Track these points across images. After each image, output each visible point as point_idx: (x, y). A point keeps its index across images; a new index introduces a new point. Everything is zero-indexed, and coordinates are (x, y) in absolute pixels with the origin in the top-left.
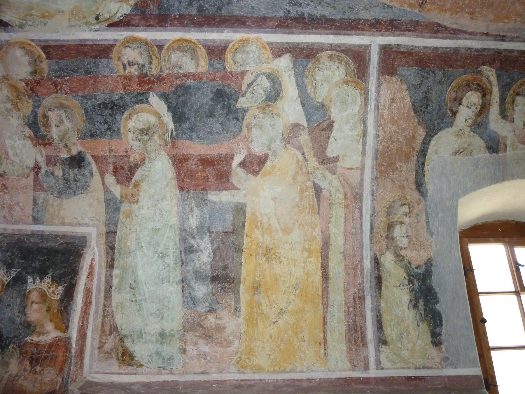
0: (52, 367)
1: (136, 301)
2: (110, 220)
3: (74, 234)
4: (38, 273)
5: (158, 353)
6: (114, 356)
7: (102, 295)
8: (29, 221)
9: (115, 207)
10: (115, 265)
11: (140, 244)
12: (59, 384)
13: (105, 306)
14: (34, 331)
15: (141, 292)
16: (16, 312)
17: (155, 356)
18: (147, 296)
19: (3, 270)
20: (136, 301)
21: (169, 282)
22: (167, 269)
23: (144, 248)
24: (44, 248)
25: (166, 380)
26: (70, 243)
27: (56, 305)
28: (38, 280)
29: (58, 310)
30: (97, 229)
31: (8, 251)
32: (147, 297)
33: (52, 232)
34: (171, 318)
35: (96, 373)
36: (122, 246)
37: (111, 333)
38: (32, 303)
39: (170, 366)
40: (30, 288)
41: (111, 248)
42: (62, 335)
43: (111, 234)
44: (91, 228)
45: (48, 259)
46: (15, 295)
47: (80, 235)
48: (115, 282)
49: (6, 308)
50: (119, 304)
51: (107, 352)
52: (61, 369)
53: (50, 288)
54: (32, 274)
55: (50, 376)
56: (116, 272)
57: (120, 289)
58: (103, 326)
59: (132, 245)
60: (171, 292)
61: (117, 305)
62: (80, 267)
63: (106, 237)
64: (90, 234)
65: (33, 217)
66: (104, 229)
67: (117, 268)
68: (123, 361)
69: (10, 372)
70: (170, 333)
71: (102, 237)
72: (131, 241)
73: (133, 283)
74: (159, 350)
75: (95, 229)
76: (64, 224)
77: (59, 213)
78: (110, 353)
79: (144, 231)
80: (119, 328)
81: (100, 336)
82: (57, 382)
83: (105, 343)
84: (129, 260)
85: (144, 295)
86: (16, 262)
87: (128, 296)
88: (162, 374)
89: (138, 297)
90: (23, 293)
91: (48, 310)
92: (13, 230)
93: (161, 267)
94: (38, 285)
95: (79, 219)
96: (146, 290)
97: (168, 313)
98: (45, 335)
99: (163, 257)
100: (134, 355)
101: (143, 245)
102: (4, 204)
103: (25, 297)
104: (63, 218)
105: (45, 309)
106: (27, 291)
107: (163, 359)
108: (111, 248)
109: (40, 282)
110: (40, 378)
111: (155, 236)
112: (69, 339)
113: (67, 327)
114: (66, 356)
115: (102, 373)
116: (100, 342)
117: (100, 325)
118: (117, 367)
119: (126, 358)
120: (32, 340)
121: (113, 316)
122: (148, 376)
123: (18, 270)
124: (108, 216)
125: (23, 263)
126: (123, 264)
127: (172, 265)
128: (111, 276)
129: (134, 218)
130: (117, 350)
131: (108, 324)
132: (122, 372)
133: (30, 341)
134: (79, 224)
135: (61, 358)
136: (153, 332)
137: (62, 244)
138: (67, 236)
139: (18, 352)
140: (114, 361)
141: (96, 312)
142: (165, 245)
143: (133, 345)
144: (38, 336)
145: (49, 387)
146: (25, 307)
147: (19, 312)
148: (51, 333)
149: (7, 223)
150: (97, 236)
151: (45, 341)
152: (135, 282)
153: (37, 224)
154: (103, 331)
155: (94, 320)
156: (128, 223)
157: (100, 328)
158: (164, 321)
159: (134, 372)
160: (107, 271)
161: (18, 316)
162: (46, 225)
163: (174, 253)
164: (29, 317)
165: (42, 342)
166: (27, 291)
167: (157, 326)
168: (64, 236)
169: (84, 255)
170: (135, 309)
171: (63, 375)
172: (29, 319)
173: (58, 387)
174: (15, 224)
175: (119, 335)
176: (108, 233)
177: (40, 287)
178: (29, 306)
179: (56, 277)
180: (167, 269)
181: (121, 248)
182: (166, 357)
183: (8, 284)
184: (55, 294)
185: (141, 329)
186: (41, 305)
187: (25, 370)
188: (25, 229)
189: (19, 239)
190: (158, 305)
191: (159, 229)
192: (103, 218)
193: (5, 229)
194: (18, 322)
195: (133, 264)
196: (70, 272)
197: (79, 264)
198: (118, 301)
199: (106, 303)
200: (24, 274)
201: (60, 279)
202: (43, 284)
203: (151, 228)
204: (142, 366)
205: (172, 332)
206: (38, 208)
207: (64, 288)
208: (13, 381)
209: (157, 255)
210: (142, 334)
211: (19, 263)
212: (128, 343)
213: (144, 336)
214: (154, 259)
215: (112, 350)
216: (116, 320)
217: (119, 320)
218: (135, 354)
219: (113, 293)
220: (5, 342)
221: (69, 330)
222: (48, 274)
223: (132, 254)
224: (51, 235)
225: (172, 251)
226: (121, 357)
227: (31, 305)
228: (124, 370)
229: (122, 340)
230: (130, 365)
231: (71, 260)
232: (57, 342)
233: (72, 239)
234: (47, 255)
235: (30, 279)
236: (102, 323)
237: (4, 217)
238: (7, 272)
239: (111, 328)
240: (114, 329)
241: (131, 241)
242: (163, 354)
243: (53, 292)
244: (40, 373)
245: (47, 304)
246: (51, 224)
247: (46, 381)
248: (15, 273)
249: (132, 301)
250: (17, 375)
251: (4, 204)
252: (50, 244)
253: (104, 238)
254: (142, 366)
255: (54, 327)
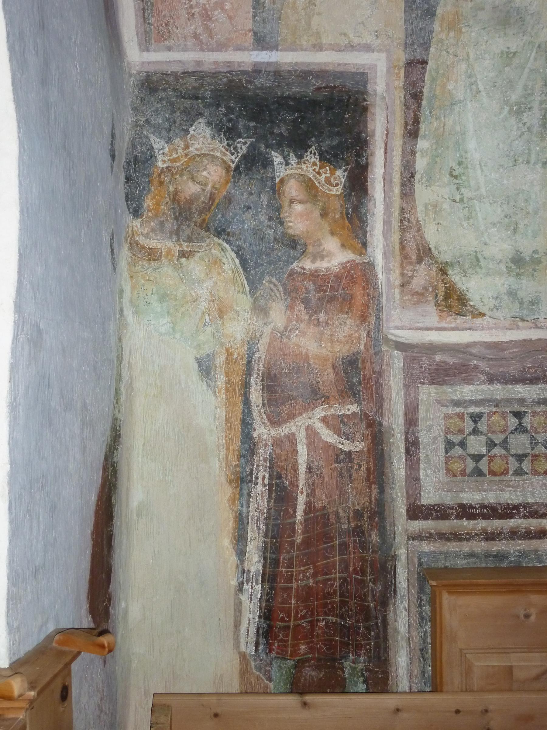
0: (347, 313)
1: (462, 200)
2: (414, 37)
3: (341, 69)
4: (289, 146)
5: (512, 293)
6: (430, 298)
7: (397, 190)
8: (247, 44)
9: (426, 6)
10: (421, 132)
11: (474, 87)
12: (363, 343)
13: (402, 210)
14: (304, 252)
15: (472, 183)
16: (263, 218)
17: (506, 297)
18: (483, 191)
19: (221, 142)
20: (462, 200)
21: (528, 162)
22: (526, 136)
23: (483, 93)
24: (288, 97)
25: (528, 338)
26: (335, 87)
27: (337, 204)
28: (293, 160)
29: (342, 213)
30: (389, 59)
31: (218, 106)
32: (485, 193)
33: (297, 64)
34: (533, 231)
35: (397, 328)
36: (437, 92)
37: (420, 260)
38: (291, 202)
39: (534, 315)
40: (282, 175)
41: (415, 96)
42: (357, 258)
43: (416, 66)
44: (376, 54)
45: (303, 118)
46: (255, 189)
47: (353, 70)
48: (421, 164)
49: (244, 213)
50: (430, 208)
51: (417, 293)
52: (364, 318)
53: (319, 173)
54: (279, 146)
55: (346, 328)
56: (422, 144)
57: (430, 180)
58: (403, 248)
59: (457, 88)
60: (532, 182)
61: (426, 209)
62: (370, 133)
63: (406, 72)
64: (374, 67)
65: (255, 34)
66: (401, 57)
67: (424, 137)
68: (446, 307)
69: (272, 324)
70: (531, 257)
71: (398, 74)
72: (456, 81)
73: (456, 167)
74: (513, 287)
75: (384, 56)
76: (319, 47)
77: (309, 24)
78: (422, 294)
79: (483, 58)
80: (433, 249)
81: (402, 265)
82: (359, 339)
83: (412, 277)
84: (450, 121)
85: (478, 188)
86: (240, 125)
87: (445, 192)
88: (518, 328)
89: (467, 193)
90: (269, 184)
91: (324, 214)
92: (216, 63)
93: (515, 133)
94: (296, 169)
95: (351, 36)
96: (482, 180)
97: (526, 222)
98: (326, 259)
99: (519, 113)
100: (467, 297)
101: (481, 88)
102: (191, 7)
103: (276, 190)
104: (318, 34)
105: (317, 213)
106: (277, 180)
107: (521, 303)
108: (415, 96)
109: (298, 163)
110: (329, 332)
111: (507, 69)
112: (370, 265)
113: (365, 245)
114: (368, 295)
115: (410, 329)
116: (402, 275)
117: (397, 246)
118: (437, 319)
119: (453, 302)
120: (303, 268)
121: (419, 230)
122: (494, 331)
123: (249, 141)
124: (410, 28)
125: (255, 127)
126: (436, 129)
127: (536, 129)
128: (413, 153)
129: (463, 30)
130: (435, 288)
131: (413, 244)
132: (446, 325)
133: (299, 270)
134: (352, 47)
135: (359, 299)
136: (499, 256)
137: (319, 89)
138: (327, 72)
139: (281, 290)
140: (431, 308)
141: (387, 223)
142: (525, 87)
143: (464, 278)
144: (313, 261)
145: (347, 347)
146: (279, 209)
147: (270, 219)
148: (335, 256)
149: (202, 50)
150: (388, 71)
151: (326, 269)
152: (460, 163)
153: (264, 49)
154: (405, 257)
155: (385, 236)
156: (452, 41)
157: (397, 252)
158: (518, 237)
159: (467, 326)
160: (404, 143)
161: (269, 226)
162: (281, 50)
163: (541, 103)
164: (289, 227)
165: (321, 271)
166: (277, 180)
167: (506, 246)
168: (322, 73)
169: (371, 109)
170: (461, 215)
171: (368, 326)
172: (290, 231)
173: (362, 347)
174: (217, 50)
175: (436, 262)
176: (410, 64)
177: (299, 171)
178: (286, 208)
179: (327, 152)
180: (526, 136)
181: (435, 96)
182: (527, 300)
183: (237, 168)
184: (331, 184)
185: (476, 252)
186: (308, 205)
187: (299, 320)
188: (240, 60)
189: (231, 81)
190: (505, 206)
191: (515, 53)
192: (398, 32)
193: (199, 63)
194: (272, 238)
195: (458, 128)
196: (351, 143)
197: (366, 127)
198: (427, 201)
199: (405, 205)
200: (263, 148)
201: (336, 156)
202: (304, 166)
203: (498, 51)
204: (482, 315)
205: (536, 256)
206: (264, 15)
207: (346, 174)
208: (282, 338)
209: (507, 109)
210: (478, 260)
211: (247, 128)
212: (455, 276)
213: (483, 263)
214: (502, 116)
215: (425, 288)
216: (426, 236)
217: (432, 236)
218: (469, 295)
219: (417, 187)
220: (253, 272)
221: (369, 249)
222: (310, 147)
223: (457, 108)
224: (295, 71)
225: (538, 99)
226: (443, 300)
227: (290, 206)
228: (450, 323)
229: (443, 271)
230: (459, 314)
231: (347, 119)
232: (349, 272)
233: (339, 78)
234: (299, 111)
235: (277, 158)
236: (401, 243)
237: (196, 36)
238: (228, 145)
239: (419, 250)
240: (425, 253)
241: (456, 81)
242: (521, 294)
243: (328, 181)
244: (327, 323)
245: (321, 204)
246: (293, 48)
247: (341, 337)
248: (244, 148)
249: (455, 201)
250: (286, 328)
251: (191, 7)
252: (294, 89)
253: (402, 74)
254: (482, 315)
255: (339, 244)
